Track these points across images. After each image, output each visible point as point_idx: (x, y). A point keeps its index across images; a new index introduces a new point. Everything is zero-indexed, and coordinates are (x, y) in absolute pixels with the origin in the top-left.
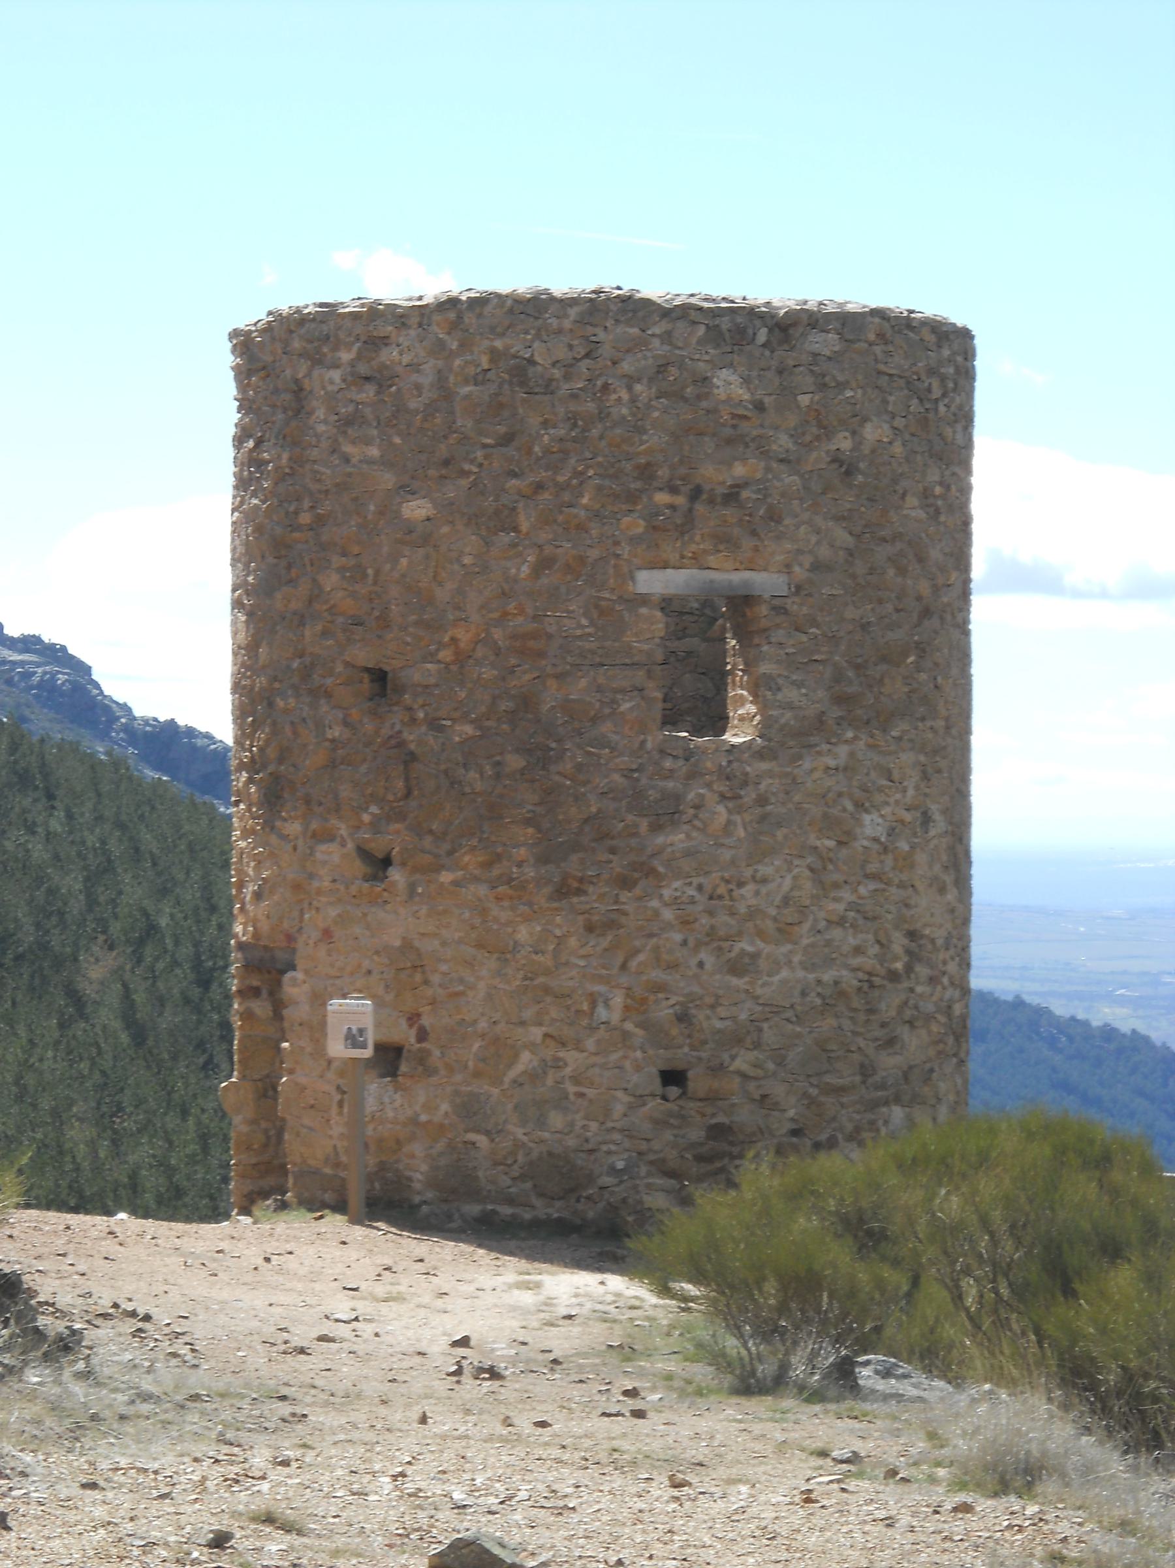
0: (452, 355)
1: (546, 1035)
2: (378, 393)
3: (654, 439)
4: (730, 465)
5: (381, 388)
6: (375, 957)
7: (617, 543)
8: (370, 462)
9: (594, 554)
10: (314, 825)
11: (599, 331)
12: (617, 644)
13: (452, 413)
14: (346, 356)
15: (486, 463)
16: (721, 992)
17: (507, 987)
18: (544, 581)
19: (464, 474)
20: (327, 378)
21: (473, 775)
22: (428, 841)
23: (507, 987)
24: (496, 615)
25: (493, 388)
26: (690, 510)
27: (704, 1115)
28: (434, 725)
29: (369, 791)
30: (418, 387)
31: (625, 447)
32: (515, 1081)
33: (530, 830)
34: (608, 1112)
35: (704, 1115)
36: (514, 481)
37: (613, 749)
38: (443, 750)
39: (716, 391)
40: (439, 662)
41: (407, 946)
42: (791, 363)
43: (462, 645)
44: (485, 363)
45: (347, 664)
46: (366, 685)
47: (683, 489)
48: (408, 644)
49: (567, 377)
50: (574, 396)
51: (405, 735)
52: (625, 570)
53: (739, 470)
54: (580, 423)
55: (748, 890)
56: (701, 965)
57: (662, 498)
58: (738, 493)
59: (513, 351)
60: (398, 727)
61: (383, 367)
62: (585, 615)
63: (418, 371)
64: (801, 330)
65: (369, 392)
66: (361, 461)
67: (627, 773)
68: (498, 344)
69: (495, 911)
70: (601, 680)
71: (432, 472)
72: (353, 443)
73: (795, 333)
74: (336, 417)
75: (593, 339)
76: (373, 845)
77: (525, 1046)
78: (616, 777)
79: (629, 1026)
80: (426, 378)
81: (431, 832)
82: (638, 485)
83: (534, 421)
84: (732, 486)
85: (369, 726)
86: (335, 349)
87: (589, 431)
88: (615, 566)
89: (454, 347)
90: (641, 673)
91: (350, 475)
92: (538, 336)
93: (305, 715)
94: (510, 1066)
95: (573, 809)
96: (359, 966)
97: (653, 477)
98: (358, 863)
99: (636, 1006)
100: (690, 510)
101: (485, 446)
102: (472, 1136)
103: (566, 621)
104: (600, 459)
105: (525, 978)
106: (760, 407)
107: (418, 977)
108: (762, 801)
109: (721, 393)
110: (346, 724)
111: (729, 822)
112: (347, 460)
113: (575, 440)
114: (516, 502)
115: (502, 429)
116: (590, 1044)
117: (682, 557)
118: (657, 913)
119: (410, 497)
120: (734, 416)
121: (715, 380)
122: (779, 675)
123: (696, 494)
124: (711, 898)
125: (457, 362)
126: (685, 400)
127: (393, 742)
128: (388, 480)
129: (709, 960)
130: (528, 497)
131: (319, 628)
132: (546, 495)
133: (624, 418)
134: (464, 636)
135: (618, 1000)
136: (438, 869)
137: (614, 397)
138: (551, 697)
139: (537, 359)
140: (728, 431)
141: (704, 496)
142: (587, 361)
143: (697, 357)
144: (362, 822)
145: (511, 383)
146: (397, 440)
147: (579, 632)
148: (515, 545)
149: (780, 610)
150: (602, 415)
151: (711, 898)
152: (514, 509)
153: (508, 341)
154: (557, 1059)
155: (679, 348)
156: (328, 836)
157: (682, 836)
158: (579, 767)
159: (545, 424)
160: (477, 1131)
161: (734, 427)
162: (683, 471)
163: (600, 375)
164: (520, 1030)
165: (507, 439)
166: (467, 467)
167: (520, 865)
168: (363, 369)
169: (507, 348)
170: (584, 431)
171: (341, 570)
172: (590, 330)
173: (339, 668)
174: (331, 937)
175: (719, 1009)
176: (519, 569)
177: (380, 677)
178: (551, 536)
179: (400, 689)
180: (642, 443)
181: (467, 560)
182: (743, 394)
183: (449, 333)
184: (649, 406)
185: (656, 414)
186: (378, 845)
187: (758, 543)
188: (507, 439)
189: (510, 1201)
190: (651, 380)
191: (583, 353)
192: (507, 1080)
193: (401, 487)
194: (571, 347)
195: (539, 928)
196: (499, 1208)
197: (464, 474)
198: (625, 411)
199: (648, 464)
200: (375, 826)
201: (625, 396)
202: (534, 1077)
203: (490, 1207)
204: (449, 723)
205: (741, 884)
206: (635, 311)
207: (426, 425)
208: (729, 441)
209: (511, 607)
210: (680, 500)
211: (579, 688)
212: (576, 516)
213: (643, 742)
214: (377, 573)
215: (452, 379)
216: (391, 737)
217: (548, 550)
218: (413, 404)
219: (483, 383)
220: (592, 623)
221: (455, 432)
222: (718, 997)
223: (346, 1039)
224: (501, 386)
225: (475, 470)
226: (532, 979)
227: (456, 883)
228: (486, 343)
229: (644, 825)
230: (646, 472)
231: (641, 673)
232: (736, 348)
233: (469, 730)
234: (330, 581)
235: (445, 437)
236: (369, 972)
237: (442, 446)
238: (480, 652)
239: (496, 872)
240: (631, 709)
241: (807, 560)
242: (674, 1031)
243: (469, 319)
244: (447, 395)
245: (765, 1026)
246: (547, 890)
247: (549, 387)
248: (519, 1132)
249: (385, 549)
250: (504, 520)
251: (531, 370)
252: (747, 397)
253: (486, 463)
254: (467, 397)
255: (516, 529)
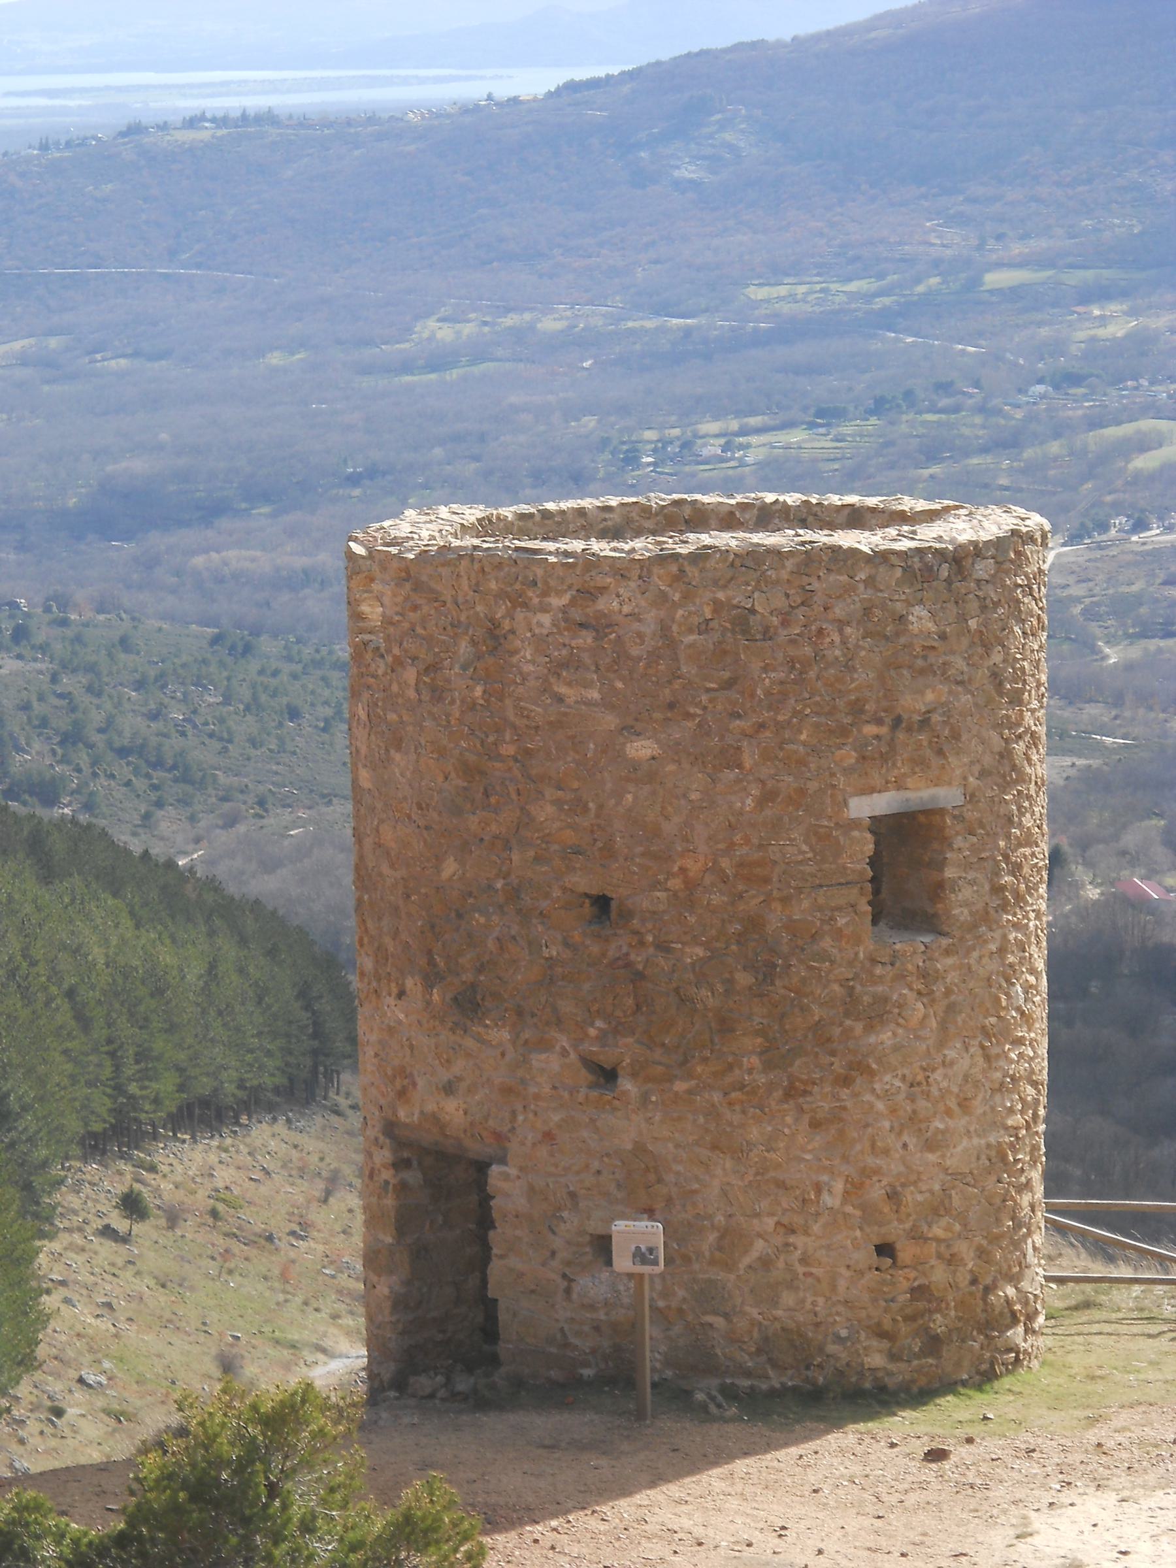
0: (675, 606)
1: (778, 1223)
2: (595, 639)
3: (863, 676)
4: (922, 693)
5: (600, 635)
6: (605, 1159)
7: (833, 775)
8: (589, 703)
9: (813, 786)
10: (527, 1035)
11: (813, 580)
12: (833, 866)
13: (677, 660)
14: (556, 602)
15: (710, 706)
16: (921, 1169)
17: (740, 1183)
18: (768, 812)
19: (689, 716)
20: (535, 621)
21: (705, 992)
22: (658, 1054)
23: (740, 1183)
24: (722, 846)
25: (716, 636)
26: (892, 739)
27: (908, 1279)
28: (663, 947)
29: (595, 1007)
30: (640, 635)
31: (838, 686)
32: (750, 1267)
33: (759, 1040)
34: (834, 1288)
35: (908, 1279)
36: (738, 722)
37: (832, 962)
38: (673, 971)
39: (911, 627)
40: (667, 890)
41: (640, 1149)
42: (963, 591)
43: (691, 874)
44: (708, 613)
45: (564, 889)
46: (587, 909)
47: (886, 720)
48: (634, 873)
49: (785, 623)
50: (793, 642)
51: (633, 957)
52: (840, 798)
53: (930, 696)
54: (798, 666)
55: (937, 1075)
56: (905, 1146)
57: (870, 730)
58: (929, 718)
59: (735, 602)
60: (625, 949)
61: (601, 615)
62: (805, 842)
63: (640, 620)
64: (970, 560)
65: (586, 639)
66: (577, 702)
67: (844, 982)
68: (721, 595)
69: (728, 1115)
70: (821, 900)
71: (657, 715)
72: (569, 684)
73: (967, 563)
74: (547, 659)
75: (808, 588)
76: (601, 1057)
77: (759, 1235)
78: (836, 987)
79: (849, 1209)
80: (649, 627)
81: (663, 1045)
82: (847, 720)
83: (756, 666)
84: (925, 713)
85: (595, 949)
86: (545, 594)
87: (806, 673)
88: (832, 796)
89: (676, 599)
90: (855, 891)
91: (565, 714)
92: (757, 588)
93: (513, 932)
94: (746, 1252)
95: (799, 1019)
96: (587, 1166)
97: (862, 711)
98: (584, 1071)
99: (854, 1189)
100: (892, 739)
101: (708, 690)
102: (709, 1319)
103: (789, 848)
104: (818, 698)
105: (757, 1174)
106: (943, 637)
107: (652, 1177)
108: (948, 992)
109: (915, 628)
110: (566, 944)
111: (925, 1017)
112: (560, 699)
113: (795, 682)
114: (739, 741)
115: (726, 675)
116: (816, 1228)
117: (887, 782)
118: (872, 1106)
119: (634, 738)
120: (924, 648)
121: (910, 617)
122: (960, 878)
123: (898, 721)
124: (912, 1085)
125: (680, 612)
126: (886, 638)
127: (620, 963)
128: (610, 721)
129: (912, 1142)
130: (751, 736)
131: (531, 853)
132: (768, 734)
133: (837, 658)
134: (694, 867)
135: (839, 1186)
136: (671, 1079)
137: (828, 640)
138: (775, 920)
139: (758, 608)
140: (920, 663)
141: (904, 725)
142: (803, 608)
143: (896, 597)
144: (587, 1035)
145: (733, 632)
146: (619, 685)
147: (800, 858)
148: (740, 781)
149: (960, 818)
150: (819, 656)
151: (912, 1085)
152: (739, 748)
153: (730, 593)
154: (787, 1245)
155: (881, 591)
156: (544, 1045)
157: (890, 1034)
158: (804, 981)
159: (765, 669)
160: (715, 1313)
161: (925, 658)
162: (885, 704)
163: (815, 620)
164: (755, 1221)
165: (729, 684)
166: (692, 710)
167: (750, 1071)
168: (576, 615)
169: (729, 599)
170: (801, 673)
171: (558, 803)
172: (806, 579)
173: (556, 893)
174: (554, 1139)
175: (920, 1184)
176: (743, 803)
177: (602, 903)
178: (772, 772)
179: (626, 915)
180: (853, 680)
181: (694, 796)
182: (931, 626)
183: (670, 586)
184: (857, 646)
185: (863, 653)
186: (606, 1058)
187: (944, 762)
188: (729, 684)
189: (748, 1374)
190: (859, 623)
191: (799, 601)
192: (742, 1266)
193: (623, 729)
194: (787, 596)
195: (770, 1129)
196: (737, 1382)
197: (689, 716)
198: (837, 653)
199: (858, 700)
200: (602, 1038)
201: (837, 638)
202: (766, 1263)
203: (728, 1381)
204: (680, 946)
205: (934, 1070)
206: (845, 561)
207: (650, 671)
208: (922, 672)
209: (737, 838)
210: (884, 730)
211: (802, 909)
212: (796, 752)
213: (856, 954)
214: (601, 807)
215: (675, 628)
216: (618, 959)
217: (770, 784)
218: (635, 651)
219: (707, 631)
220: (812, 849)
221: (679, 677)
222: (919, 1173)
223: (634, 1256)
224: (723, 635)
225: (699, 712)
226: (763, 1174)
227: (690, 1092)
228: (709, 595)
229: (859, 1027)
230: (857, 708)
231: (855, 891)
232: (925, 585)
233: (700, 952)
234: (544, 812)
235: (669, 682)
236: (599, 1172)
237: (667, 691)
238: (708, 880)
239: (729, 1079)
240: (847, 924)
241: (976, 769)
242: (886, 1210)
243: (692, 571)
244: (671, 644)
245: (953, 1192)
246: (778, 1094)
247: (767, 634)
248: (754, 1312)
249: (609, 786)
250: (730, 758)
251: (752, 618)
252: (934, 629)
253: (710, 706)
254: (691, 646)
255: (740, 766)
